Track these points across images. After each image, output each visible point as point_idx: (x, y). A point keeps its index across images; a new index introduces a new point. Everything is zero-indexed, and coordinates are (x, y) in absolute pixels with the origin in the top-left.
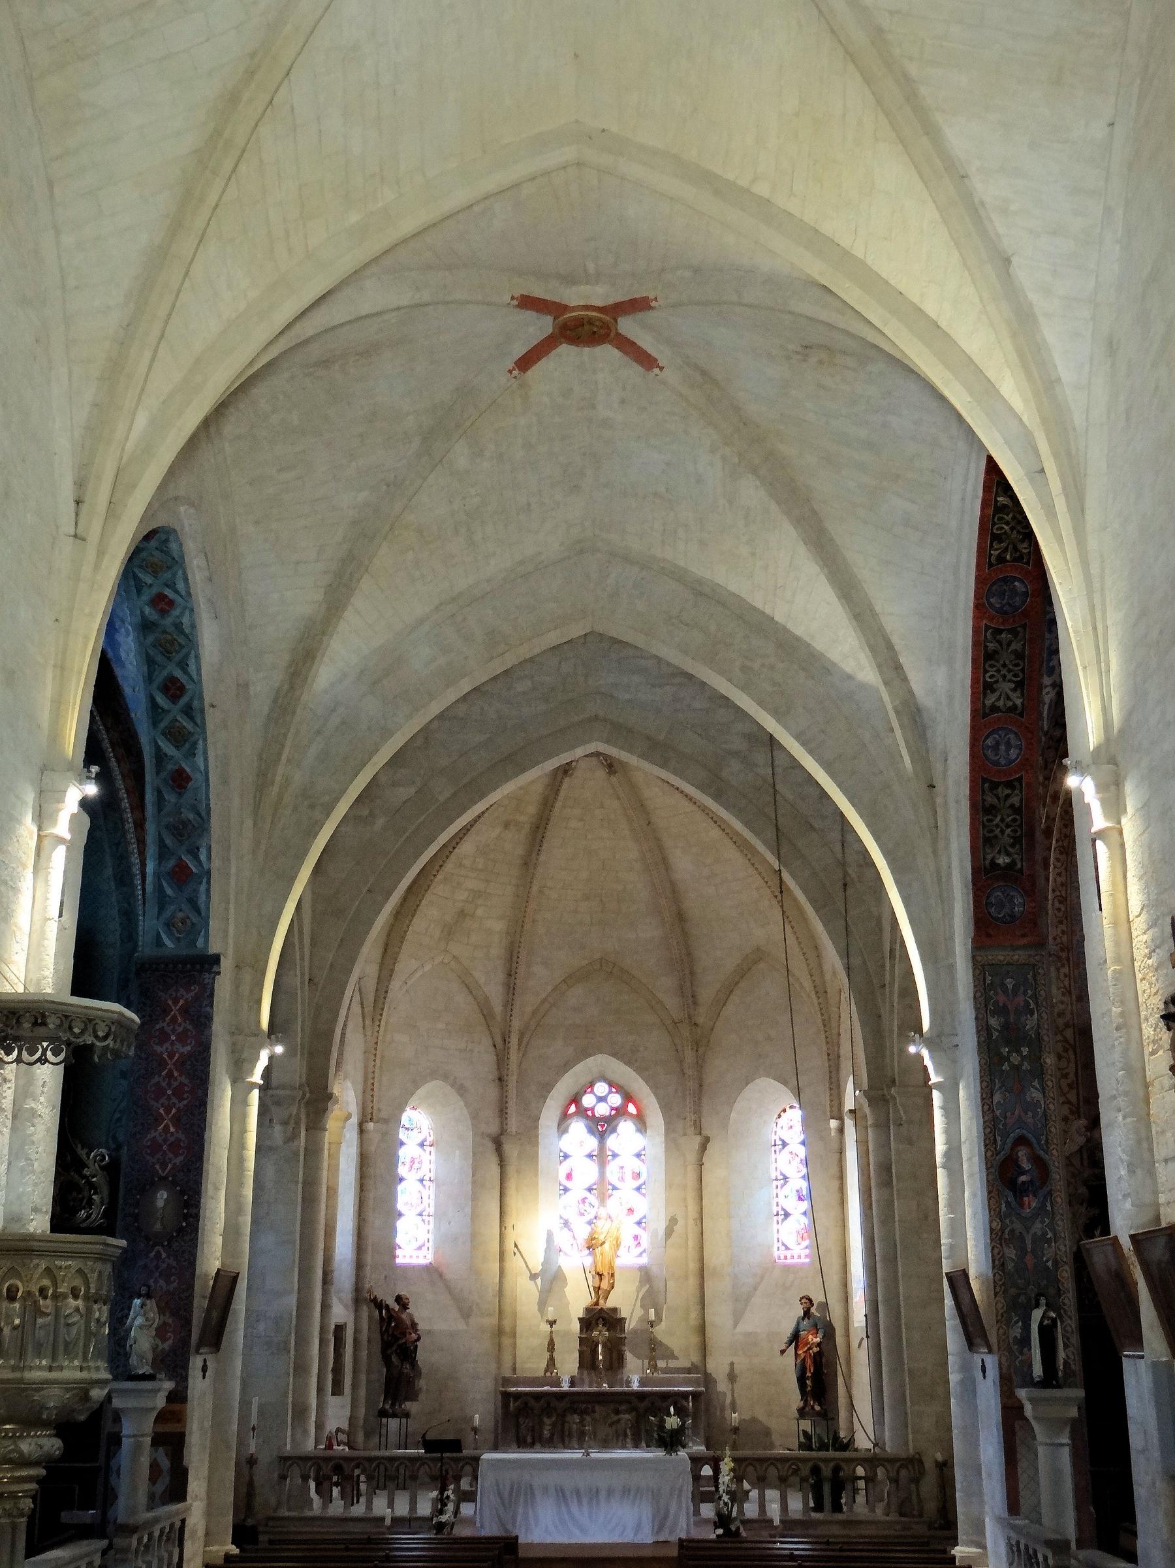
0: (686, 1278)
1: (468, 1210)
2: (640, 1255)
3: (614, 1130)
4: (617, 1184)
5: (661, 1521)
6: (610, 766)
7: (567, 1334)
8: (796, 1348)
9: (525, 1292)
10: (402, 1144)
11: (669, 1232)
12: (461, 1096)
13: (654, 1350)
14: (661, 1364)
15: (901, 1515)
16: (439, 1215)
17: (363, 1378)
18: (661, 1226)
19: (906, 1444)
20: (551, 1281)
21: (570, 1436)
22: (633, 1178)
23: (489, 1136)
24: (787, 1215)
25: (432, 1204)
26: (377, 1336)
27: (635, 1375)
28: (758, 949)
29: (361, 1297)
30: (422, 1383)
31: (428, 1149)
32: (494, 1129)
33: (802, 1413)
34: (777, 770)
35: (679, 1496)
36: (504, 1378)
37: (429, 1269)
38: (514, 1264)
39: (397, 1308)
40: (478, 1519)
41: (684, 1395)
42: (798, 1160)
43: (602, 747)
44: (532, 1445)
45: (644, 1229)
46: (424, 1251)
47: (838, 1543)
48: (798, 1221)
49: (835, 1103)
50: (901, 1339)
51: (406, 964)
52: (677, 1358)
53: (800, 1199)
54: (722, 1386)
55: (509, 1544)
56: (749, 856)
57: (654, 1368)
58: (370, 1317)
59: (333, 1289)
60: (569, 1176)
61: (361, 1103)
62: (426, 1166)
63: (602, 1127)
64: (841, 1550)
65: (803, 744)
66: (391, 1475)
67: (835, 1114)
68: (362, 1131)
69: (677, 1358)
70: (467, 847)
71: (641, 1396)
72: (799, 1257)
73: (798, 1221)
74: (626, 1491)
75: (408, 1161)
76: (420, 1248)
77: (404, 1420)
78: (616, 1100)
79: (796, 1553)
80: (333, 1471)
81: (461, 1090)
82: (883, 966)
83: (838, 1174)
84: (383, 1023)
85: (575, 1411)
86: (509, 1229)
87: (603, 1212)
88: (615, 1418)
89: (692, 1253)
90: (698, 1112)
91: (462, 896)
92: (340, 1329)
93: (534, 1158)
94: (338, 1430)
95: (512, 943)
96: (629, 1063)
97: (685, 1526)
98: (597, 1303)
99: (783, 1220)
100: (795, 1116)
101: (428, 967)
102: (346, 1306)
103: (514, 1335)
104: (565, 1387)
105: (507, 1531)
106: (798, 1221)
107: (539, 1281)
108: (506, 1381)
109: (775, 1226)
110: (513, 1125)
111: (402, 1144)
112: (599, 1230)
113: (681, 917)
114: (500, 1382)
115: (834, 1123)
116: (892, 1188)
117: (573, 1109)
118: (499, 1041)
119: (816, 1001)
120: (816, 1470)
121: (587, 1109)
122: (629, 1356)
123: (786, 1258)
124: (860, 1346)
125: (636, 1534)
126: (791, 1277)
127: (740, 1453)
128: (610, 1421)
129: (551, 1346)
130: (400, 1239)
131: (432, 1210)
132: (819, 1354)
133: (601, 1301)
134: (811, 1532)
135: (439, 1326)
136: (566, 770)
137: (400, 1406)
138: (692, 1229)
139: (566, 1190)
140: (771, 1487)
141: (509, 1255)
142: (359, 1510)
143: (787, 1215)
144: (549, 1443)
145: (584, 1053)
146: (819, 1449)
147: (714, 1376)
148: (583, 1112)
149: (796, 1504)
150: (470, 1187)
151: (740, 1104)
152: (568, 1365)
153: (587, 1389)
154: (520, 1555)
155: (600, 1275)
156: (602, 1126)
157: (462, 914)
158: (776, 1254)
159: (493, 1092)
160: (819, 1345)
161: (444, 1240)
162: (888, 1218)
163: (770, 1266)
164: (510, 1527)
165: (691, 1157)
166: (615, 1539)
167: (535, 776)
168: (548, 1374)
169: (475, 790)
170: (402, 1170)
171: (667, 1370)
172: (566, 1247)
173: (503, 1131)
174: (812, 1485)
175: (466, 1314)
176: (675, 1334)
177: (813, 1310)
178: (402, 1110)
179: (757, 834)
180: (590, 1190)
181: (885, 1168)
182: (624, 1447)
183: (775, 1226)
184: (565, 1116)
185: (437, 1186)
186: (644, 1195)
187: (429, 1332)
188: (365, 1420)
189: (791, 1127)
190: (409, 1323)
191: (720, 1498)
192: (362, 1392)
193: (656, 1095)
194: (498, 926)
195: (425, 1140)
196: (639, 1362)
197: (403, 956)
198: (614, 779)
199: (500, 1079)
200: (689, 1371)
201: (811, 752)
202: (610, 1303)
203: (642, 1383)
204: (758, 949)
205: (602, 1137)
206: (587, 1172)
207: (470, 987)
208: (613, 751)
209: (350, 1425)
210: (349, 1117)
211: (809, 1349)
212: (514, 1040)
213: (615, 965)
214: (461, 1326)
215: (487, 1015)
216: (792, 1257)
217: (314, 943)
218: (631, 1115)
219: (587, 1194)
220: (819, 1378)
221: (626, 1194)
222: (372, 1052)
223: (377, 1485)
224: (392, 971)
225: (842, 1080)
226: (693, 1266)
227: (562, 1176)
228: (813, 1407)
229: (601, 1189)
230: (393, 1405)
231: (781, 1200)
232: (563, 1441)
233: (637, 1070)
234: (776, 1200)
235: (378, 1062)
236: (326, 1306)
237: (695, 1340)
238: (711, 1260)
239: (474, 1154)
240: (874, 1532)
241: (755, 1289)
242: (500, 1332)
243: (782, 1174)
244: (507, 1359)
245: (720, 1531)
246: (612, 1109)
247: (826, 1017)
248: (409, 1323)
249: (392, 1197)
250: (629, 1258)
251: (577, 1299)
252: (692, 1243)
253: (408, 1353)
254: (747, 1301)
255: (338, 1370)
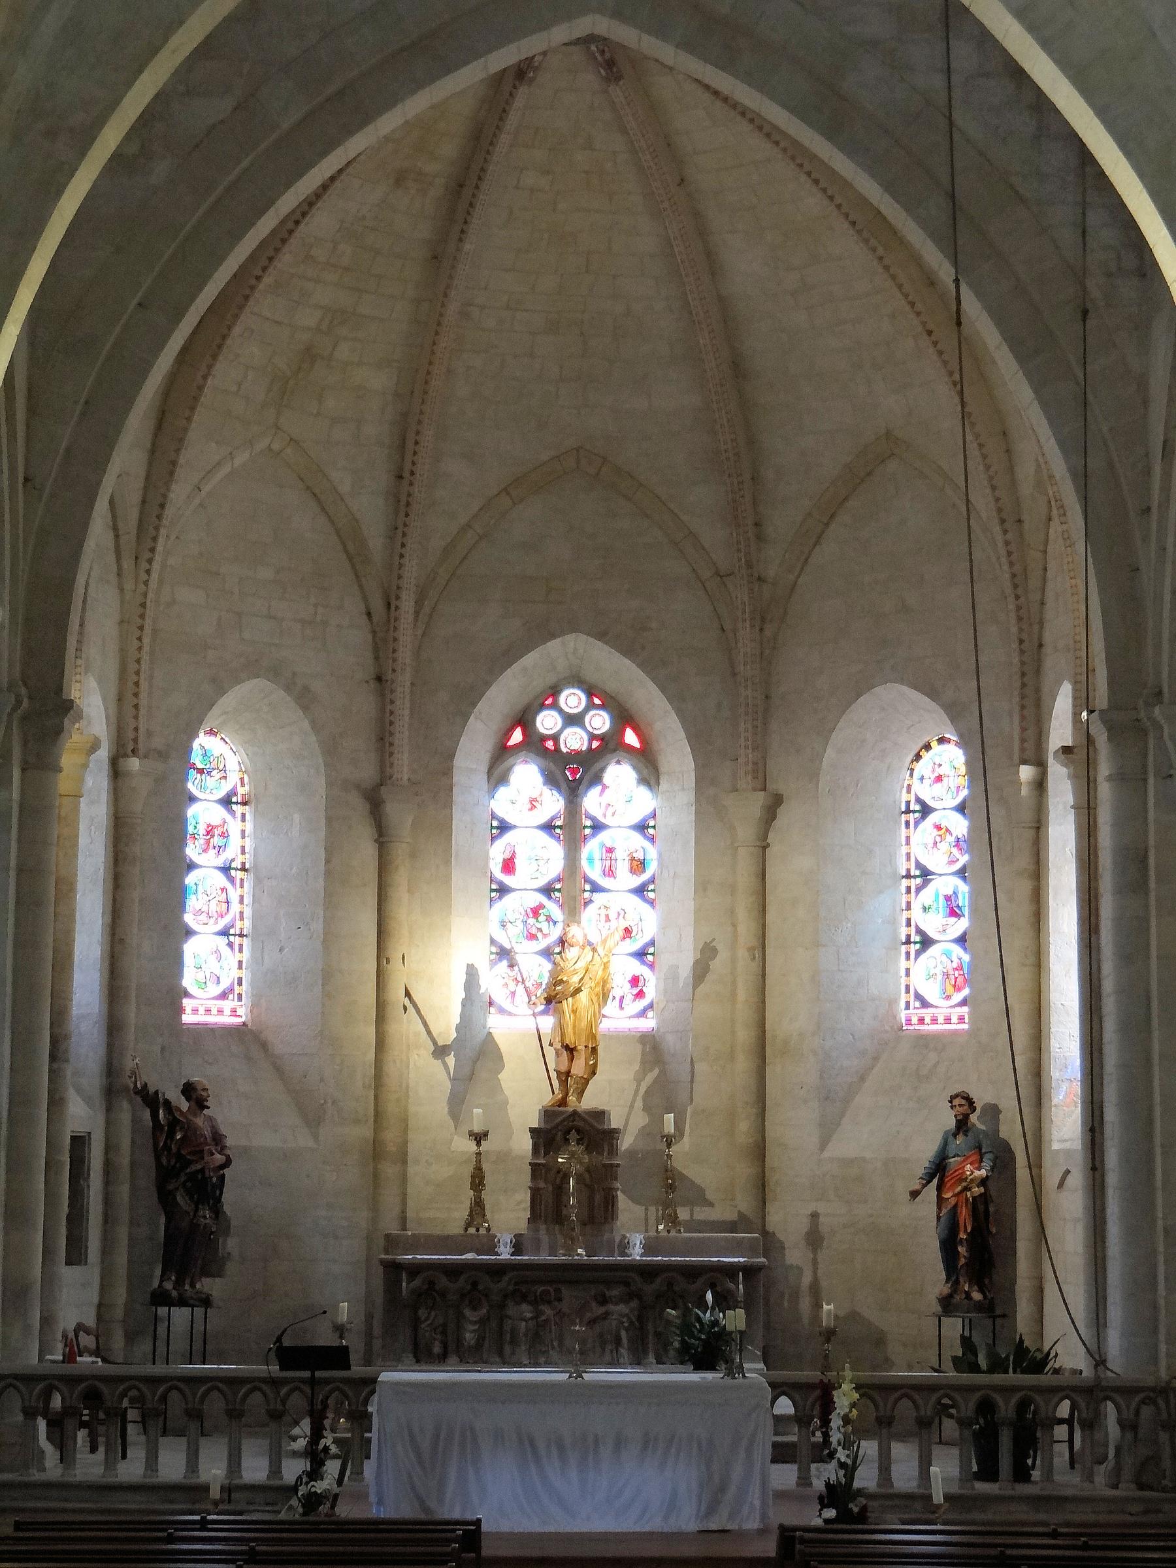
0: (732, 1057)
1: (318, 926)
2: (642, 1014)
3: (597, 779)
4: (603, 882)
5: (714, 1494)
6: (610, 64)
7: (504, 1157)
8: (940, 1188)
9: (425, 1080)
10: (192, 799)
11: (701, 971)
12: (305, 708)
13: (671, 1188)
14: (683, 1214)
15: (1141, 1487)
16: (262, 934)
17: (122, 1233)
18: (685, 961)
19: (1155, 1359)
20: (474, 1057)
21: (514, 1342)
22: (633, 871)
23: (357, 787)
24: (926, 942)
25: (248, 912)
26: (150, 1160)
27: (635, 1236)
28: (888, 434)
29: (116, 1085)
30: (231, 1244)
31: (238, 809)
32: (367, 772)
33: (947, 1305)
34: (955, 78)
35: (749, 1451)
36: (387, 1236)
37: (238, 1033)
38: (405, 1027)
39: (184, 1105)
40: (380, 1492)
41: (730, 1271)
42: (950, 839)
43: (602, 25)
44: (442, 1358)
45: (651, 966)
46: (227, 1005)
47: (1082, 1535)
48: (946, 956)
49: (1031, 733)
50: (1151, 1173)
51: (200, 451)
52: (711, 1205)
53: (953, 913)
54: (795, 1255)
55: (472, 1534)
56: (881, 251)
57: (673, 1221)
58: (135, 1120)
59: (69, 1071)
60: (509, 866)
61: (113, 719)
62: (235, 842)
63: (573, 773)
64: (1086, 1546)
65: (1032, 28)
66: (172, 1406)
67: (1030, 754)
68: (116, 772)
69: (711, 1205)
70: (321, 222)
71: (647, 1272)
72: (948, 1020)
73: (948, 955)
74: (647, 1443)
75: (202, 830)
76: (223, 996)
77: (199, 1311)
78: (600, 721)
79: (1009, 1552)
80: (91, 1404)
81: (304, 699)
82: (1148, 471)
83: (1032, 867)
84: (156, 566)
85: (524, 1298)
86: (396, 963)
87: (575, 932)
88: (602, 1310)
89: (744, 1011)
90: (761, 748)
91: (308, 318)
92: (79, 1143)
93: (444, 829)
94: (79, 1328)
95: (405, 415)
96: (628, 651)
97: (757, 1503)
98: (563, 1102)
99: (918, 954)
100: (950, 758)
101: (241, 458)
102: (88, 1100)
103: (402, 1158)
104: (505, 1254)
105: (427, 1510)
106: (948, 955)
107: (451, 1060)
108: (391, 1242)
109: (903, 964)
110: (404, 765)
111: (192, 799)
112: (568, 966)
113: (739, 369)
114: (382, 1242)
115: (1026, 772)
116: (1147, 894)
117: (517, 736)
118: (377, 605)
119: (999, 538)
120: (986, 1407)
121: (544, 738)
122: (622, 1199)
123: (921, 1021)
124: (1061, 1184)
125: (666, 1518)
126: (933, 1057)
127: (865, 1375)
128: (588, 1315)
129: (478, 1181)
130: (188, 980)
131: (247, 925)
132: (985, 1198)
133: (572, 1099)
134: (977, 1516)
135: (265, 1140)
136: (522, 72)
137: (193, 1285)
138: (745, 967)
139: (503, 890)
140: (902, 1438)
141: (395, 1011)
142: (132, 1469)
143: (926, 942)
144: (473, 1356)
145: (541, 632)
146: (991, 1370)
147: (781, 1236)
148: (536, 745)
149: (946, 1471)
150: (321, 883)
151: (843, 733)
152: (509, 1213)
153: (544, 1257)
154: (483, 1553)
155: (570, 1050)
156: (574, 772)
157: (309, 356)
158: (903, 1015)
159: (366, 703)
160: (983, 1182)
161: (268, 982)
162: (1134, 950)
163: (892, 1036)
164: (432, 1504)
165: (746, 832)
166: (627, 1524)
167: (468, 79)
168: (472, 1230)
169: (352, 108)
170: (192, 851)
171: (692, 1226)
172: (500, 997)
173: (384, 778)
174: (975, 1433)
175: (313, 1118)
176: (707, 1160)
177: (973, 1118)
178: (194, 735)
179: (910, 206)
180: (547, 890)
181: (1134, 860)
182: (614, 1363)
183: (903, 964)
184: (502, 755)
185: (258, 881)
186: (652, 903)
187: (246, 1150)
188: (128, 1310)
189: (939, 779)
190: (207, 1132)
191: (832, 1455)
192: (121, 1259)
193: (680, 713)
194: (379, 381)
195: (233, 792)
196: (639, 1210)
197: (194, 434)
198: (617, 93)
199: (379, 679)
200: (732, 1227)
201: (1046, 44)
202: (590, 1100)
203: (648, 1248)
204: (888, 434)
205: (573, 792)
206: (541, 858)
207: (320, 496)
208: (625, 34)
209: (99, 1318)
210: (94, 747)
211: (967, 1189)
212: (407, 604)
213: (605, 459)
214: (304, 1140)
215: (354, 553)
216: (934, 1021)
217: (32, 411)
218: (630, 749)
219: (542, 899)
220: (980, 1242)
221: (618, 898)
222: (134, 621)
223: (157, 1421)
224: (174, 463)
225: (1045, 690)
226: (744, 1035)
227: (496, 868)
228: (968, 1296)
229: (570, 890)
230: (179, 1283)
231: (916, 915)
232: (501, 1353)
233: (641, 665)
234: (905, 915)
235: (146, 641)
236: (56, 1102)
237: (744, 1170)
238: (781, 1025)
239: (329, 820)
240: (1091, 1518)
241: (863, 1079)
242: (376, 1151)
243: (918, 865)
244: (389, 1197)
245: (831, 1513)
246: (593, 737)
247: (1017, 568)
248: (207, 1132)
249: (177, 897)
250: (621, 1019)
251: (524, 1094)
252: (743, 993)
253: (208, 1190)
254: (847, 1100)
255: (77, 1217)
